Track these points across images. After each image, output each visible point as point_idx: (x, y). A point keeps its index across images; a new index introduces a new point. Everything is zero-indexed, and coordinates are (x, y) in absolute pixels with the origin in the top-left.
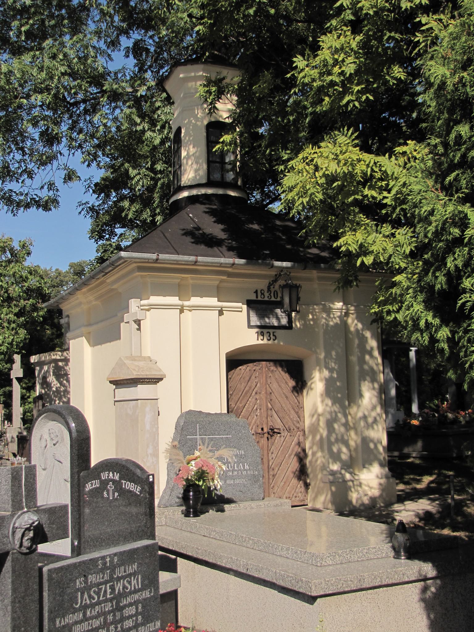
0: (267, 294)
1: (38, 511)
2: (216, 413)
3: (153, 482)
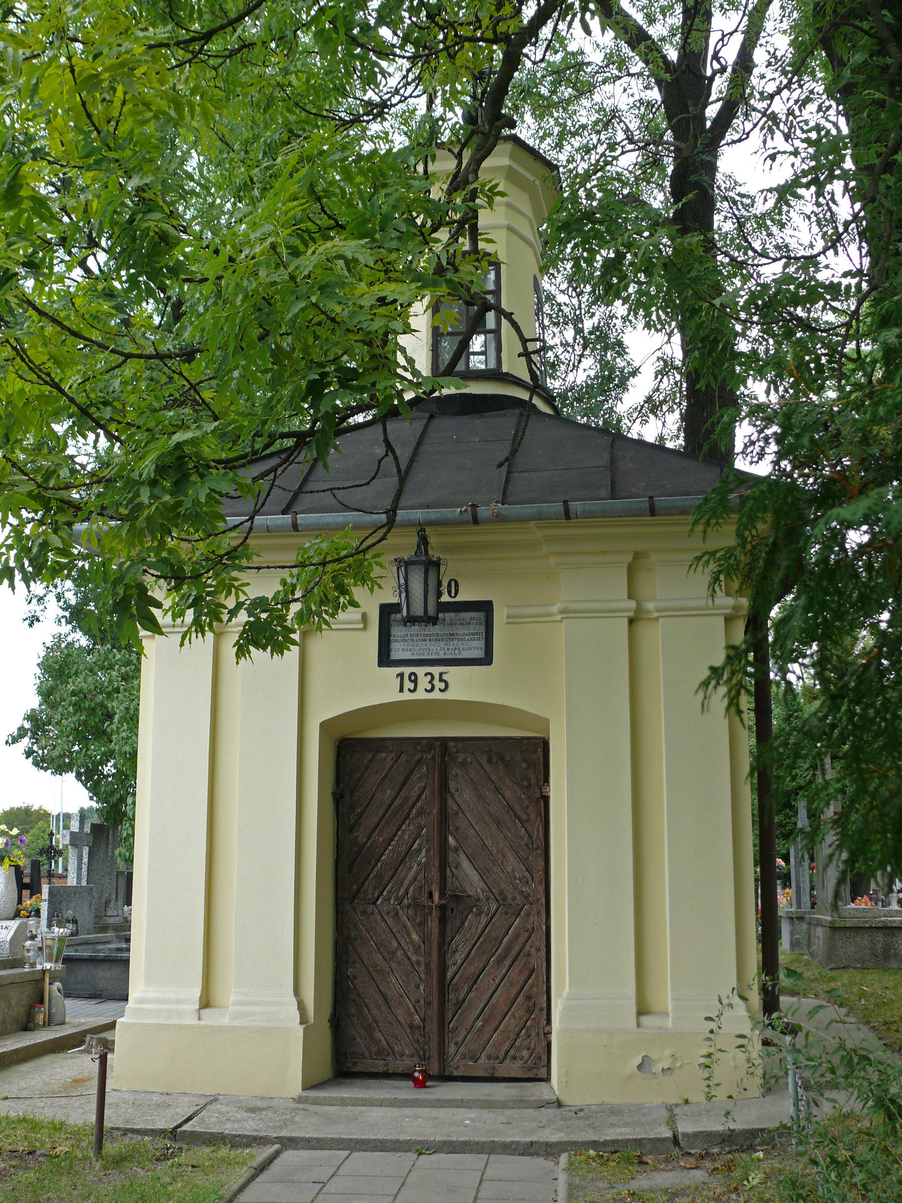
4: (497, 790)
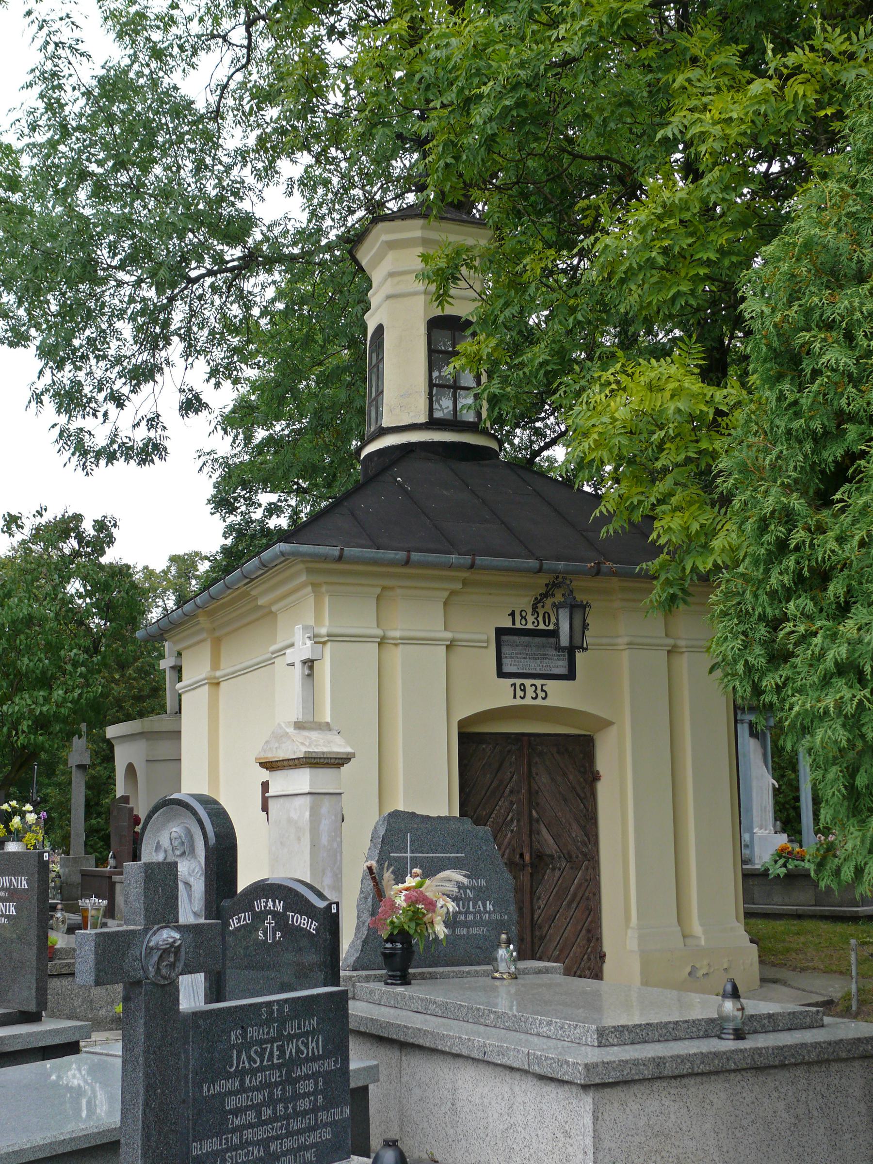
0: (531, 619)
1: (179, 928)
2: (439, 817)
3: (337, 915)
4: (565, 774)
